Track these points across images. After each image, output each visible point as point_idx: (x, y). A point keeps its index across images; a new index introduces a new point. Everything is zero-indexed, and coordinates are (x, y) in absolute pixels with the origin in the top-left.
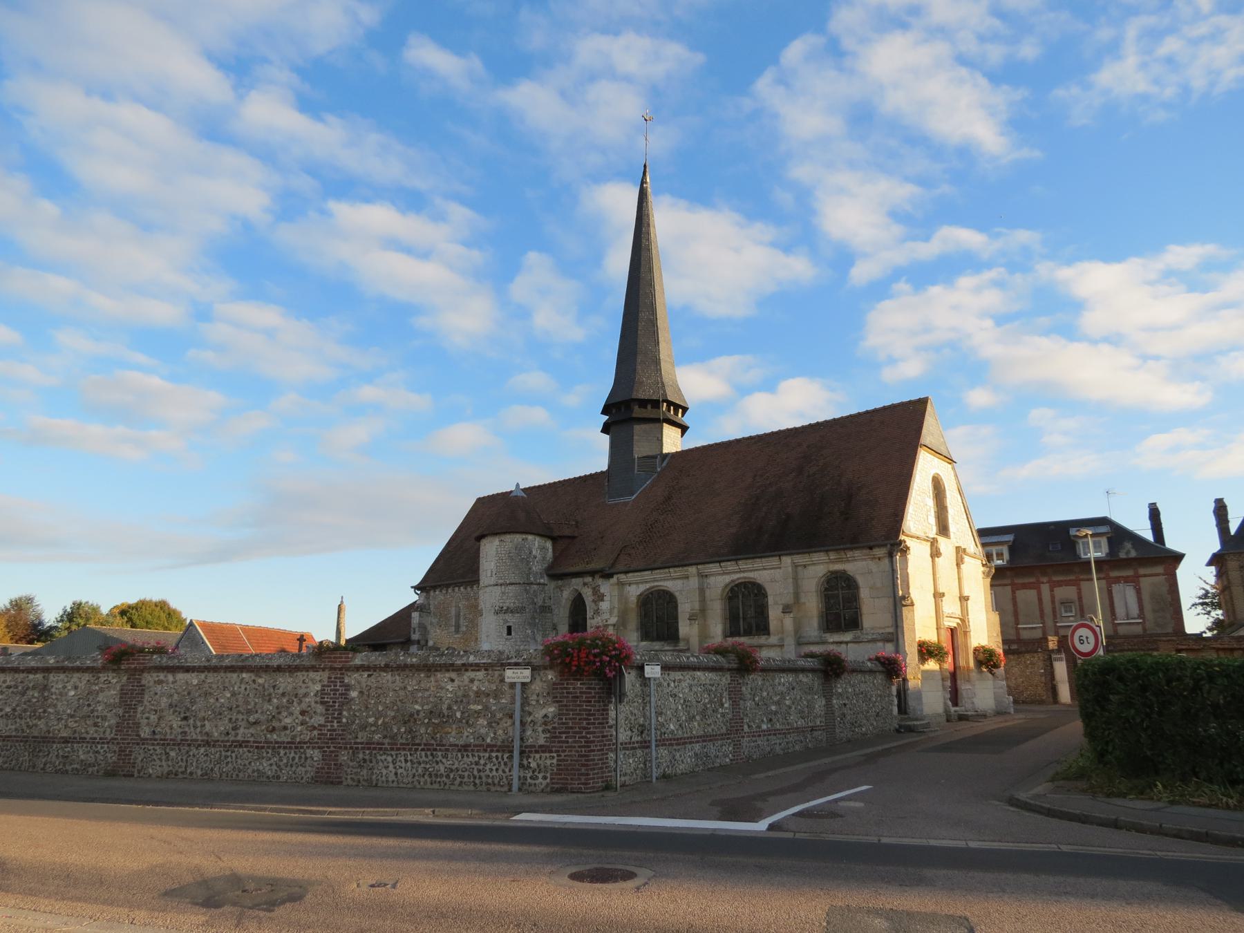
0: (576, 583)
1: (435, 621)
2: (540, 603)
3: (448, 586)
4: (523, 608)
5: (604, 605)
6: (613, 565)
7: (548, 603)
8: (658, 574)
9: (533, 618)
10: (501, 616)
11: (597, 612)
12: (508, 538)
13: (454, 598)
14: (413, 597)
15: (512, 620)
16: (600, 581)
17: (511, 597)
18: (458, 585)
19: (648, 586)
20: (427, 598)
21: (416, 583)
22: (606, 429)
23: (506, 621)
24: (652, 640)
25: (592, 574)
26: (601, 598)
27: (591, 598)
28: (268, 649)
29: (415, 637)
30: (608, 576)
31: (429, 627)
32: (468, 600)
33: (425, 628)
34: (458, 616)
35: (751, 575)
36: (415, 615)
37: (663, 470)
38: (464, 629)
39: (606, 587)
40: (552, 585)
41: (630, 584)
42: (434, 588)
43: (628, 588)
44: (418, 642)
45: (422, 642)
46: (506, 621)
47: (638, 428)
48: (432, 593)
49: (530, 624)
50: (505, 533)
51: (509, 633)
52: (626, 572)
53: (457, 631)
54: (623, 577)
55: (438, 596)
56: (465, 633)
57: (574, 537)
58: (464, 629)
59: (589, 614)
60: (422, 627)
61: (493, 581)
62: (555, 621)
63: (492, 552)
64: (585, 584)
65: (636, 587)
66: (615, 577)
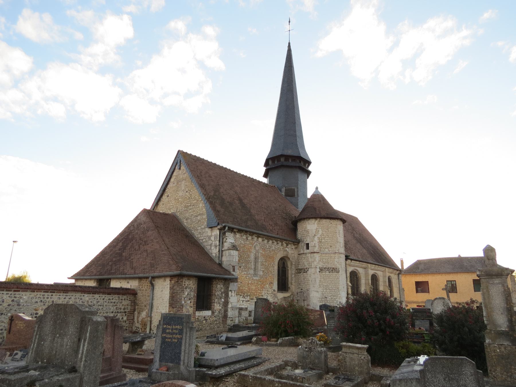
32: (264, 250)
53: (255, 274)
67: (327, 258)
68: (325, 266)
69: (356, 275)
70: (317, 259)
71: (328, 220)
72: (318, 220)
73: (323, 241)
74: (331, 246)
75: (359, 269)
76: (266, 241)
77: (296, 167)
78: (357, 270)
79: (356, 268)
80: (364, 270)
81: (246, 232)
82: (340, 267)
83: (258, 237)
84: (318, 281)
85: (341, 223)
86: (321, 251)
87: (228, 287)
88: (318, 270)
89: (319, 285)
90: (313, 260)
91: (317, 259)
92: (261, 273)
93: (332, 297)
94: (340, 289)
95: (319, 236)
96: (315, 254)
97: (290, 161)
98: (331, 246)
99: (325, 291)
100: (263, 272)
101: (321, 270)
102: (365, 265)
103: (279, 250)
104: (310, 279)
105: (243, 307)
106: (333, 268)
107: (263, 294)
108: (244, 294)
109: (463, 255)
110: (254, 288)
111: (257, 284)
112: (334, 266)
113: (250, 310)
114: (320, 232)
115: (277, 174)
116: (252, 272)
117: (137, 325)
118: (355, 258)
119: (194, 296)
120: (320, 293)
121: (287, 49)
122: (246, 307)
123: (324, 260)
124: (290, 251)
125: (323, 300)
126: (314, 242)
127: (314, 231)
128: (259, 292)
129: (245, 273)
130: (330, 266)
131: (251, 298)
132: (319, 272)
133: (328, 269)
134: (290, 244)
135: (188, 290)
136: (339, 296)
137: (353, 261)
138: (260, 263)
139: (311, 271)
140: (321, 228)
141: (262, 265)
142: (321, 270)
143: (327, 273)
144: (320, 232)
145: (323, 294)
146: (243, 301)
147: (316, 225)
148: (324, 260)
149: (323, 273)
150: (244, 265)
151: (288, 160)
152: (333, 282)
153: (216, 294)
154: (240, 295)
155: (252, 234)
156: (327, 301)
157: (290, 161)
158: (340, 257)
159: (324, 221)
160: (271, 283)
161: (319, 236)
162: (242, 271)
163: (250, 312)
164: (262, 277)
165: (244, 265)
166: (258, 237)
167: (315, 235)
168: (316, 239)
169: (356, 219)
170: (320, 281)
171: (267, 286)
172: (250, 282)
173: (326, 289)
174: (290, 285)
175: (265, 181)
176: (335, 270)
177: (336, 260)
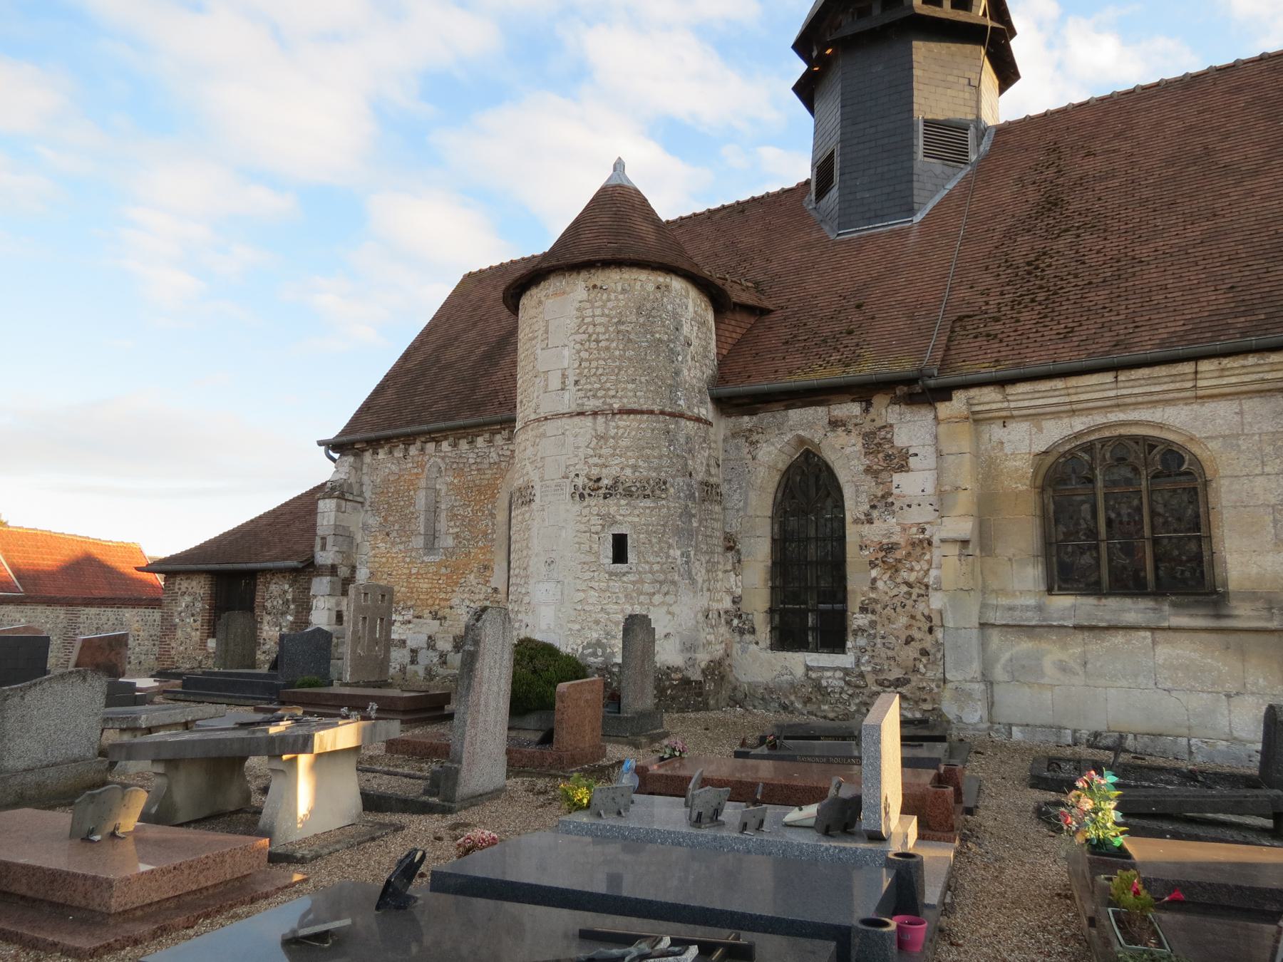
0: (805, 422)
1: (373, 521)
2: (700, 476)
3: (408, 439)
4: (662, 484)
5: (913, 484)
6: (945, 365)
7: (717, 477)
8: (1135, 383)
9: (687, 514)
10: (595, 504)
11: (884, 502)
12: (614, 279)
13: (431, 470)
14: (323, 470)
15: (630, 517)
16: (887, 412)
17: (627, 450)
18: (435, 436)
19: (1079, 424)
20: (357, 469)
21: (331, 433)
22: (806, 90)
23: (609, 520)
24: (1094, 589)
25: (864, 391)
26: (900, 461)
27: (859, 464)
28: (49, 561)
29: (325, 557)
30: (922, 392)
31: (359, 538)
32: (459, 472)
33: (350, 538)
34: (433, 510)
35: (1156, 415)
36: (327, 507)
37: (985, 159)
38: (450, 542)
39: (911, 428)
40: (722, 427)
41: (1005, 421)
42: (374, 444)
43: (997, 432)
44: (333, 570)
45: (344, 572)
46: (609, 520)
47: (924, 52)
48: (368, 457)
49: (678, 532)
50: (607, 264)
51: (620, 554)
52: (1002, 383)
53: (430, 547)
54: (988, 397)
55: (383, 464)
56: (450, 552)
57: (762, 312)
58: (450, 542)
59: (854, 506)
60: (344, 535)
61: (568, 401)
62: (734, 526)
63: (557, 326)
64: (834, 424)
65: (1029, 430)
66: (959, 397)
76: (464, 445)
78: (1161, 426)
81: (388, 439)
83: (437, 441)
87: (309, 589)
100: (457, 536)
107: (455, 601)
109: (1011, 119)
110: (424, 585)
111: (436, 573)
116: (419, 542)
117: (391, 671)
119: (203, 609)
122: (403, 637)
128: (443, 596)
129: (402, 547)
135: (188, 599)
136: (526, 599)
138: (443, 515)
141: (453, 517)
150: (397, 527)
153: (268, 604)
160: (486, 568)
162: (394, 544)
163: (414, 652)
164: (453, 554)
165: (397, 527)
166: (437, 441)
172: (414, 571)
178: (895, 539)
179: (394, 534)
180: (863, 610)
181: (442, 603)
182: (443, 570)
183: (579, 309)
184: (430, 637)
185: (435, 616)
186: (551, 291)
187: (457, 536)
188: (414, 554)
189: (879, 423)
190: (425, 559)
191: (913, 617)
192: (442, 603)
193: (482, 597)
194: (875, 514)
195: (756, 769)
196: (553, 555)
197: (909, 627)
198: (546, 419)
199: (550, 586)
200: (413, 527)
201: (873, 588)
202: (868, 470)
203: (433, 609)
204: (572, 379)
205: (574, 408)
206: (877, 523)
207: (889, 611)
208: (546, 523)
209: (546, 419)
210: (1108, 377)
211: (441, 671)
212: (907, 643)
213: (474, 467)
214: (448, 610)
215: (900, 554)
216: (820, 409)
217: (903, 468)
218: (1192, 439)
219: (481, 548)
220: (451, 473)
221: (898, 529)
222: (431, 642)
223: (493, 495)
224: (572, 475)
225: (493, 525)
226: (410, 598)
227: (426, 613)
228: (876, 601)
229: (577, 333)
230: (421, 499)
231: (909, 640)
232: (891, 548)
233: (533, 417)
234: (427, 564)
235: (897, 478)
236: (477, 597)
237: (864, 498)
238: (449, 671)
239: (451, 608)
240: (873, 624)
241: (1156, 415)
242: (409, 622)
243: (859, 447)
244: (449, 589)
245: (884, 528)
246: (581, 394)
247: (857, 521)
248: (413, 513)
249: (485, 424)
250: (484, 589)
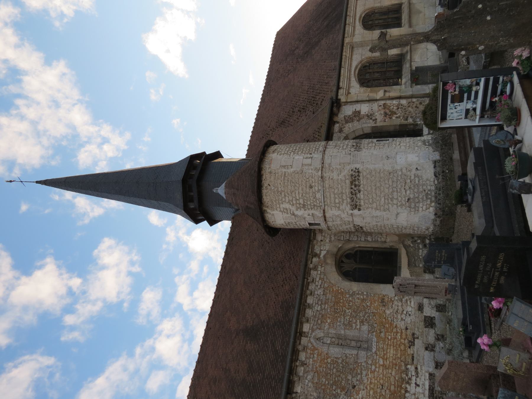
8: (345, 64)
11: (370, 116)
26: (357, 114)
52: (338, 88)
67: (332, 196)
68: (349, 200)
69: (365, 66)
70: (336, 212)
71: (264, 191)
72: (264, 208)
73: (301, 201)
74: (311, 187)
75: (354, 64)
77: (199, 186)
78: (361, 16)
79: (353, 72)
80: (356, 51)
82: (348, 168)
84: (378, 213)
85: (273, 148)
86: (320, 206)
88: (356, 212)
89: (384, 211)
90: (339, 219)
91: (336, 212)
92: (365, 328)
93: (407, 187)
94: (390, 169)
95: (293, 209)
96: (327, 215)
97: (192, 194)
98: (311, 187)
99: (395, 202)
100: (362, 322)
101: (355, 206)
102: (346, 52)
103: (326, 279)
104: (374, 223)
105: (427, 387)
106: (352, 183)
108: (403, 380)
110: (391, 352)
112: (348, 182)
113: (433, 365)
114: (287, 206)
115: (216, 211)
118: (335, 81)
120: (400, 210)
121: (44, 186)
123: (337, 201)
124: (324, 247)
125: (413, 205)
126: (306, 216)
127: (285, 215)
129: (364, 373)
130: (348, 191)
131: (410, 361)
132: (359, 210)
133: (354, 194)
134: (313, 248)
136: (404, 171)
137: (341, 84)
138: (348, 332)
139: (358, 221)
140: (279, 204)
142: (355, 206)
143: (361, 196)
144: (287, 206)
145: (402, 205)
146: (417, 385)
147: (275, 212)
148: (337, 201)
149: (362, 203)
150: (350, 377)
151: (192, 186)
152: (378, 185)
154: (406, 391)
155: (292, 371)
156: (415, 198)
157: (192, 194)
158: (330, 165)
159: (266, 199)
160: (383, 301)
161: (293, 209)
162: (361, 381)
167: (293, 214)
168: (300, 213)
169: (279, 34)
170: (376, 209)
171: (388, 312)
173: (392, 199)
174: (387, 245)
175: (225, 226)
176: (355, 178)
177: (335, 175)
178: (382, 112)
179: (354, 380)
180: (407, 120)
181: (404, 336)
182: (382, 335)
183: (280, 155)
184: (426, 349)
185: (412, 344)
186: (267, 166)
187: (362, 322)
188: (370, 362)
189: (343, 119)
190: (374, 350)
191: (409, 106)
192: (404, 336)
193: (400, 304)
194: (374, 118)
195: (465, 82)
196: (384, 156)
197: (412, 108)
198: (323, 163)
199: (398, 157)
200: (352, 360)
201: (399, 117)
202: (358, 121)
203: (407, 345)
204: (309, 156)
205: (321, 154)
206: (377, 117)
207: (407, 113)
208: (370, 160)
209: (323, 163)
210: (348, 17)
211: (448, 340)
212: (418, 108)
213: (323, 306)
214: (408, 331)
215: (387, 111)
216: (334, 135)
217: (359, 112)
218: (361, 62)
219: (371, 304)
220: (323, 325)
221: (379, 112)
222: (430, 348)
223: (342, 293)
224: (350, 152)
225: (358, 294)
226: (400, 366)
227: (410, 351)
228: (403, 117)
229: (290, 155)
230: (335, 351)
231: (416, 107)
232: (386, 114)
233: (320, 173)
234: (378, 349)
235: (362, 113)
236: (400, 308)
237: (368, 121)
238: (448, 333)
239: (407, 329)
240: (412, 117)
241: (354, 64)
242: (416, 368)
243: (350, 124)
244: (395, 330)
245: (379, 117)
246: (316, 152)
247: (375, 123)
248: (343, 360)
249: (302, 289)
250: (396, 303)
